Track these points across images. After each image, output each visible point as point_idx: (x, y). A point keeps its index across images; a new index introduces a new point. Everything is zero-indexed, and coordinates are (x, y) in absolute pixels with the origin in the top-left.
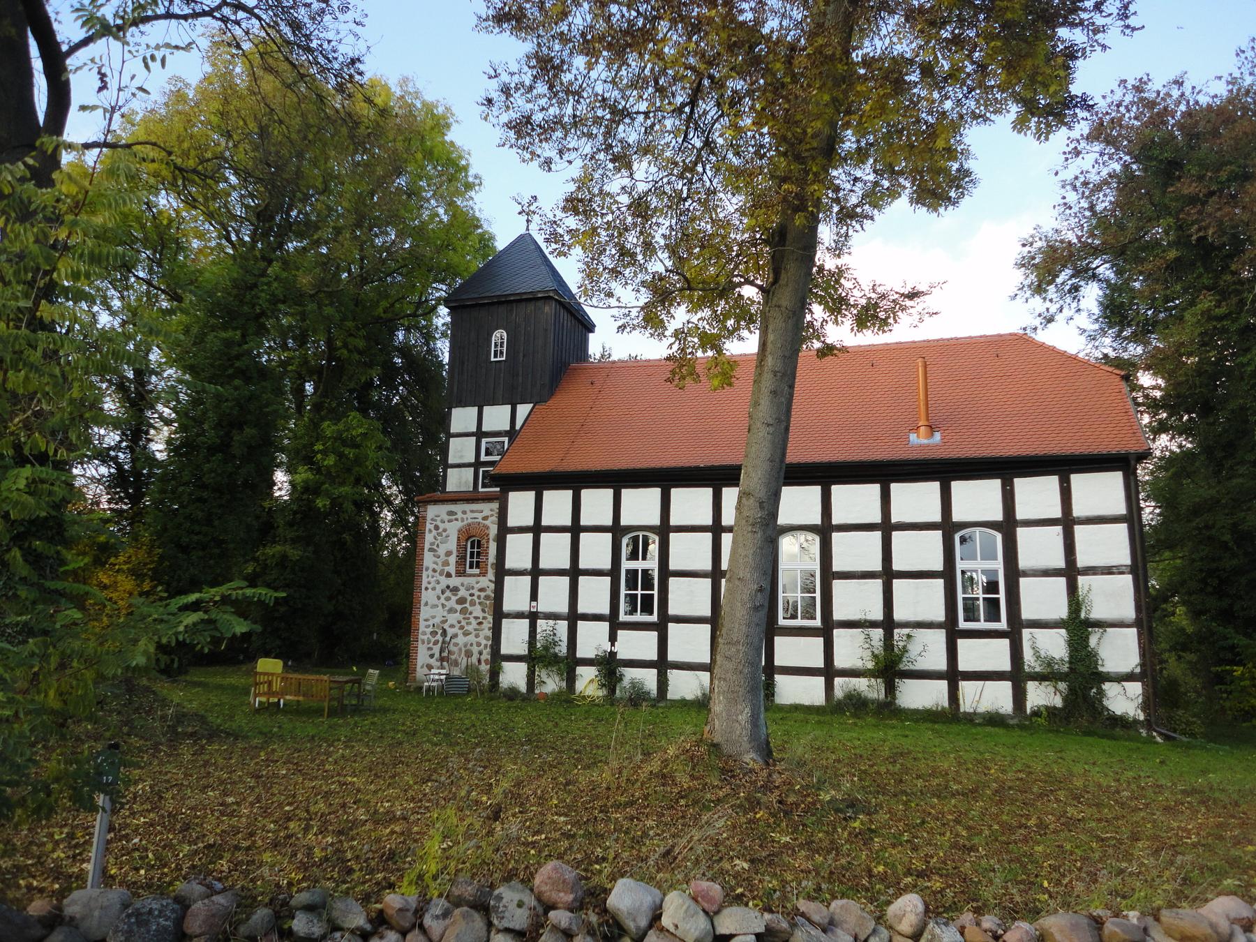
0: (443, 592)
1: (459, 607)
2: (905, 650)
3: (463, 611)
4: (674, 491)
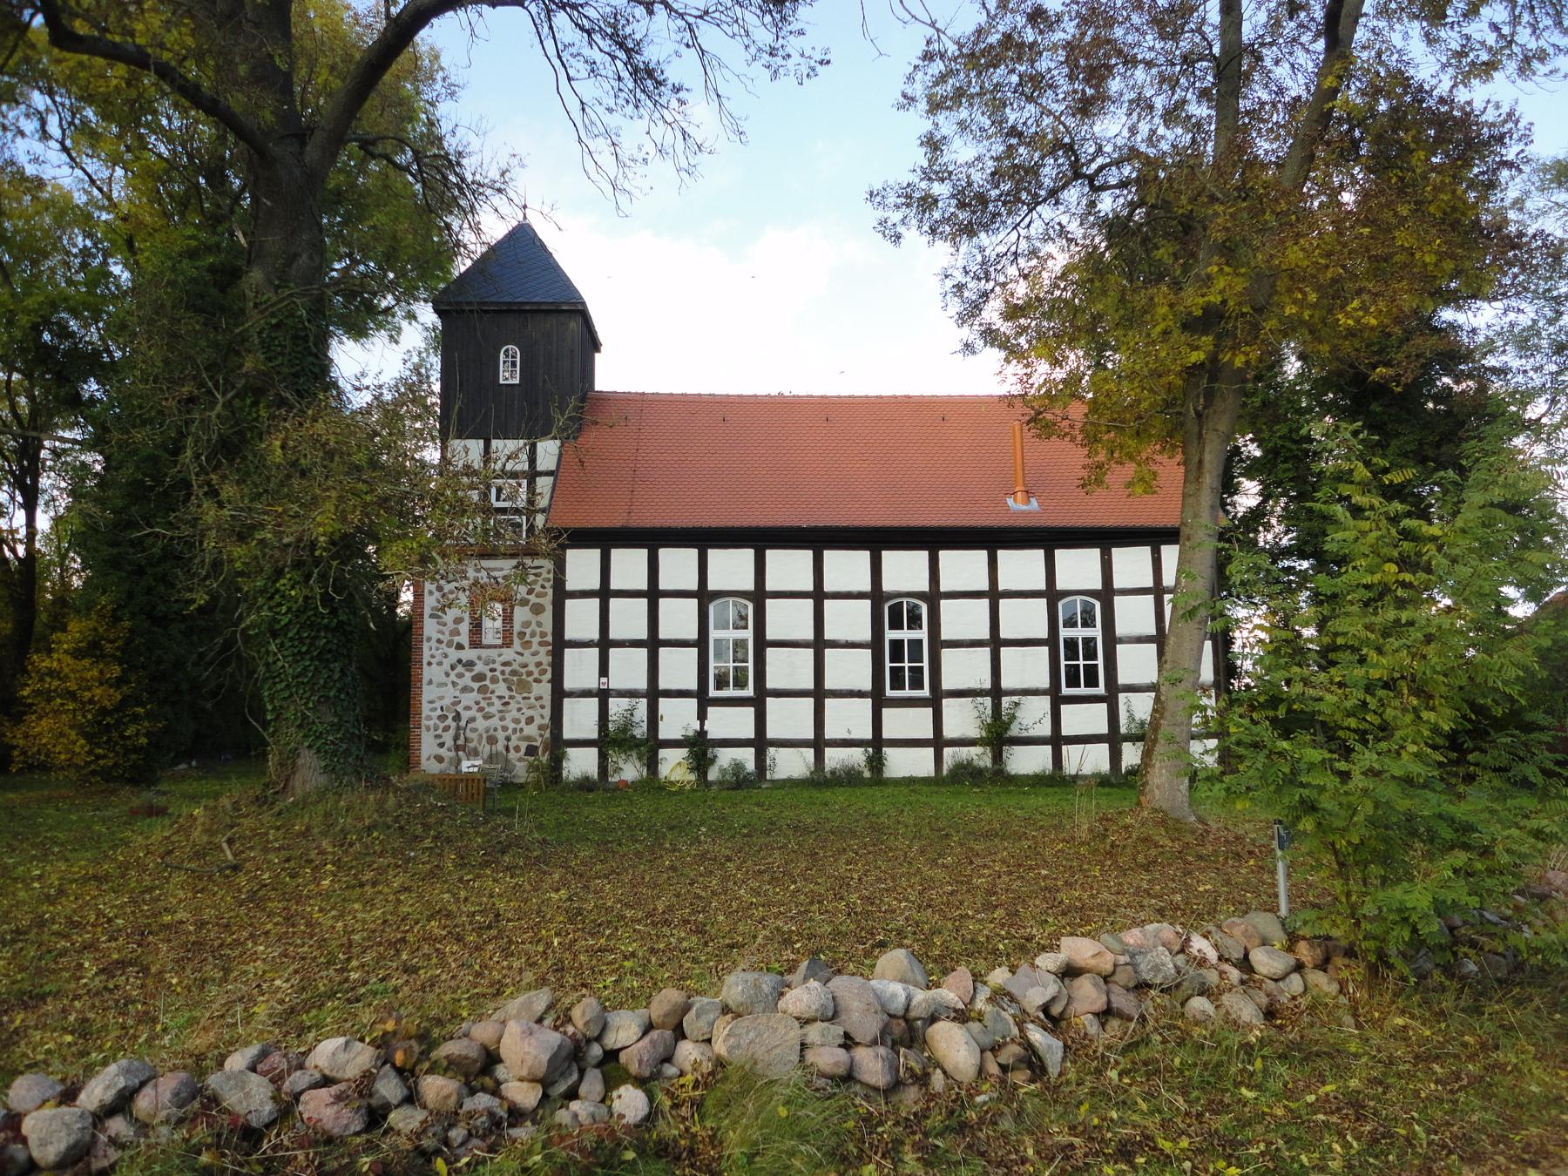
0: (453, 668)
1: (476, 685)
2: (1013, 717)
3: (482, 690)
4: (827, 553)
